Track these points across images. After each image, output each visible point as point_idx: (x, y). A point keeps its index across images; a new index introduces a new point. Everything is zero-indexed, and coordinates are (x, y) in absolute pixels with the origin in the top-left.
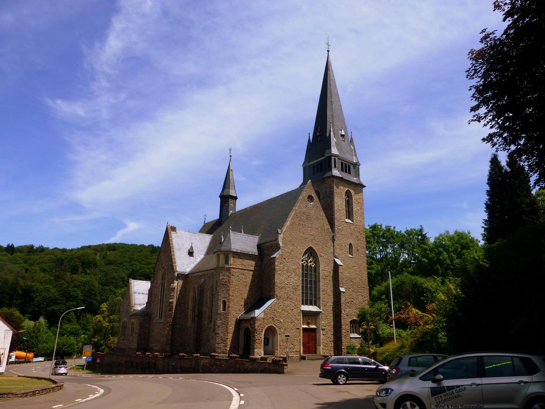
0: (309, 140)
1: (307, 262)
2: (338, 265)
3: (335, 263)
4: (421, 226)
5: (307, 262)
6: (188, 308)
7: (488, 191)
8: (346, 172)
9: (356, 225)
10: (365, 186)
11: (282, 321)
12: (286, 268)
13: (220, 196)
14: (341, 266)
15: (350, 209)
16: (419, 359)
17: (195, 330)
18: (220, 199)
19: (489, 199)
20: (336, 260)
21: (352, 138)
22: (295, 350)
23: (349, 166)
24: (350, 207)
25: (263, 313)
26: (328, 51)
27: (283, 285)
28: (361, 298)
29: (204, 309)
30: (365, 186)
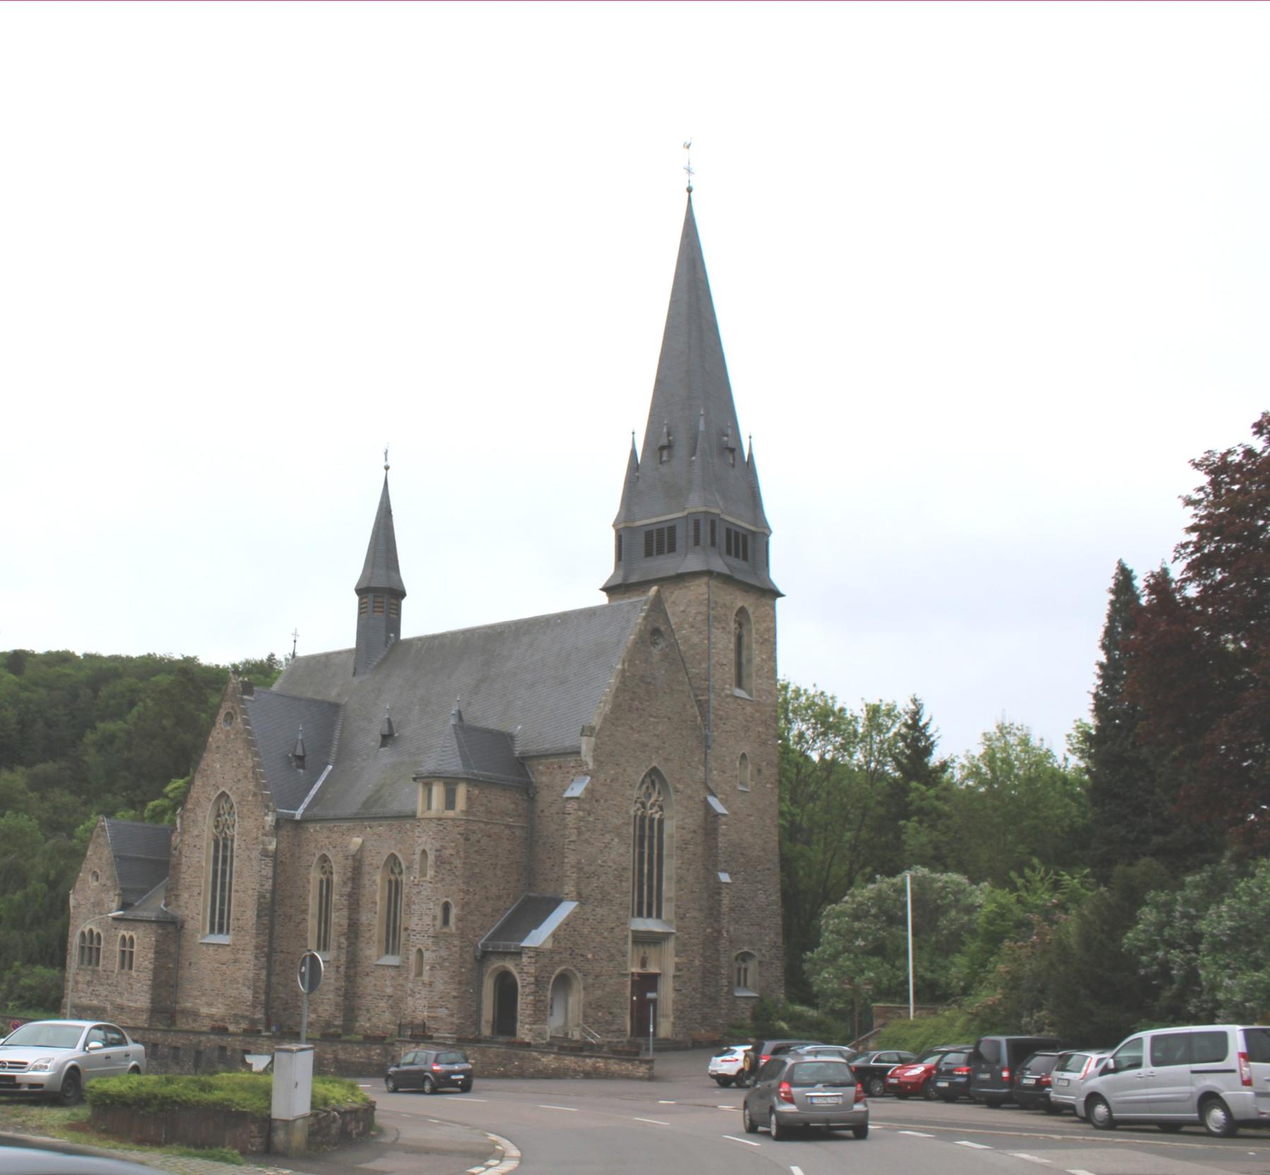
0: (633, 453)
1: (643, 805)
2: (717, 815)
3: (708, 806)
4: (914, 701)
5: (643, 805)
6: (305, 912)
7: (1101, 666)
8: (737, 556)
9: (759, 703)
10: (781, 595)
11: (590, 956)
12: (600, 826)
13: (360, 591)
14: (724, 815)
15: (744, 661)
16: (815, 1101)
17: (342, 969)
18: (356, 598)
19: (1103, 685)
20: (711, 800)
21: (751, 456)
22: (615, 1027)
23: (745, 538)
24: (745, 653)
25: (551, 940)
26: (689, 190)
27: (593, 868)
28: (762, 897)
29: (364, 917)
30: (781, 595)
